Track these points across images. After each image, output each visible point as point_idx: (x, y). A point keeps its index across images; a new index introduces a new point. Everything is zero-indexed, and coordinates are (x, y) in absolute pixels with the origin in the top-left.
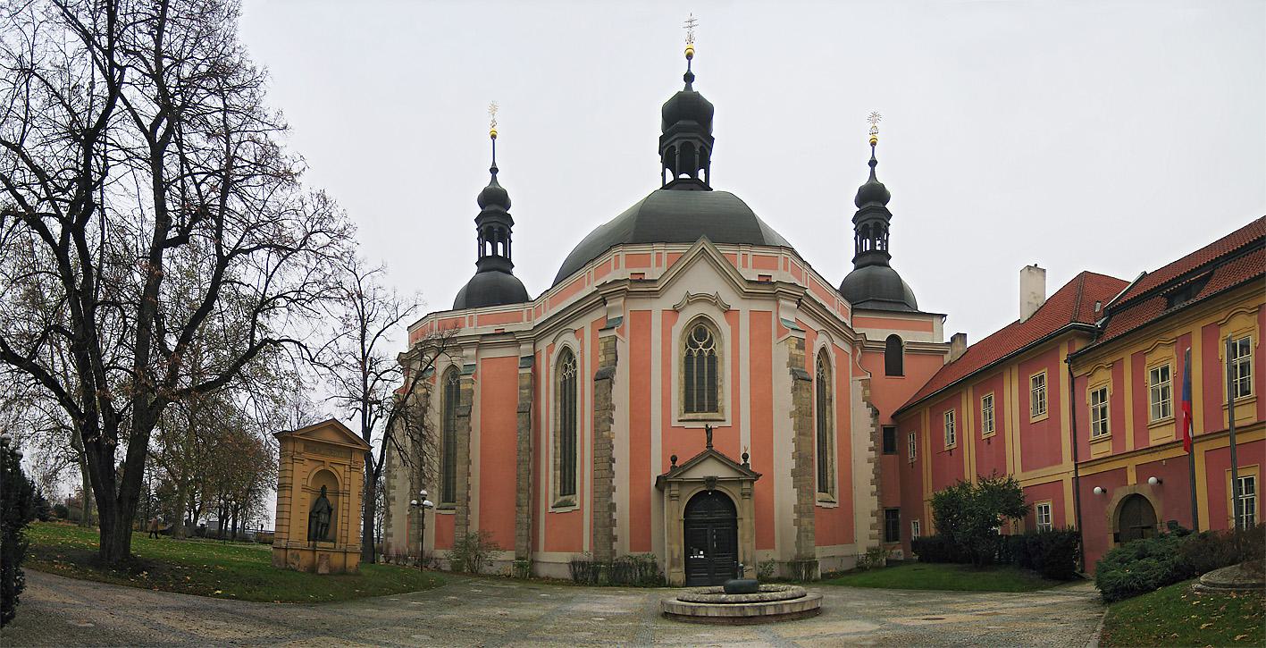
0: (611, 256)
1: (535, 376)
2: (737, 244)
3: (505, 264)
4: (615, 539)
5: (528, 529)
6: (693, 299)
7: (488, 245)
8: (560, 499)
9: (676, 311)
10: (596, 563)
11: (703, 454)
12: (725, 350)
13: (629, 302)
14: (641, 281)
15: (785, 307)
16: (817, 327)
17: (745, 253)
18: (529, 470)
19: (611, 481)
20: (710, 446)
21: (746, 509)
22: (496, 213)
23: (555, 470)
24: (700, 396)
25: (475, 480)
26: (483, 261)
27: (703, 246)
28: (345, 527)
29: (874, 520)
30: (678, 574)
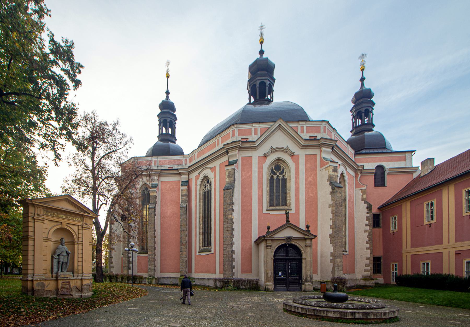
0: (230, 130)
1: (189, 190)
2: (298, 121)
3: (172, 138)
4: (234, 267)
5: (186, 263)
6: (274, 150)
7: (164, 129)
8: (202, 248)
9: (265, 156)
10: (224, 279)
11: (284, 225)
12: (291, 175)
13: (241, 152)
14: (247, 142)
15: (326, 152)
16: (340, 162)
17: (256, 127)
18: (186, 235)
19: (233, 240)
20: (288, 221)
21: (308, 254)
22: (168, 113)
23: (200, 235)
24: (278, 198)
25: (158, 239)
26: (162, 137)
27: (280, 123)
28: (80, 264)
29: (368, 262)
30: (271, 285)
